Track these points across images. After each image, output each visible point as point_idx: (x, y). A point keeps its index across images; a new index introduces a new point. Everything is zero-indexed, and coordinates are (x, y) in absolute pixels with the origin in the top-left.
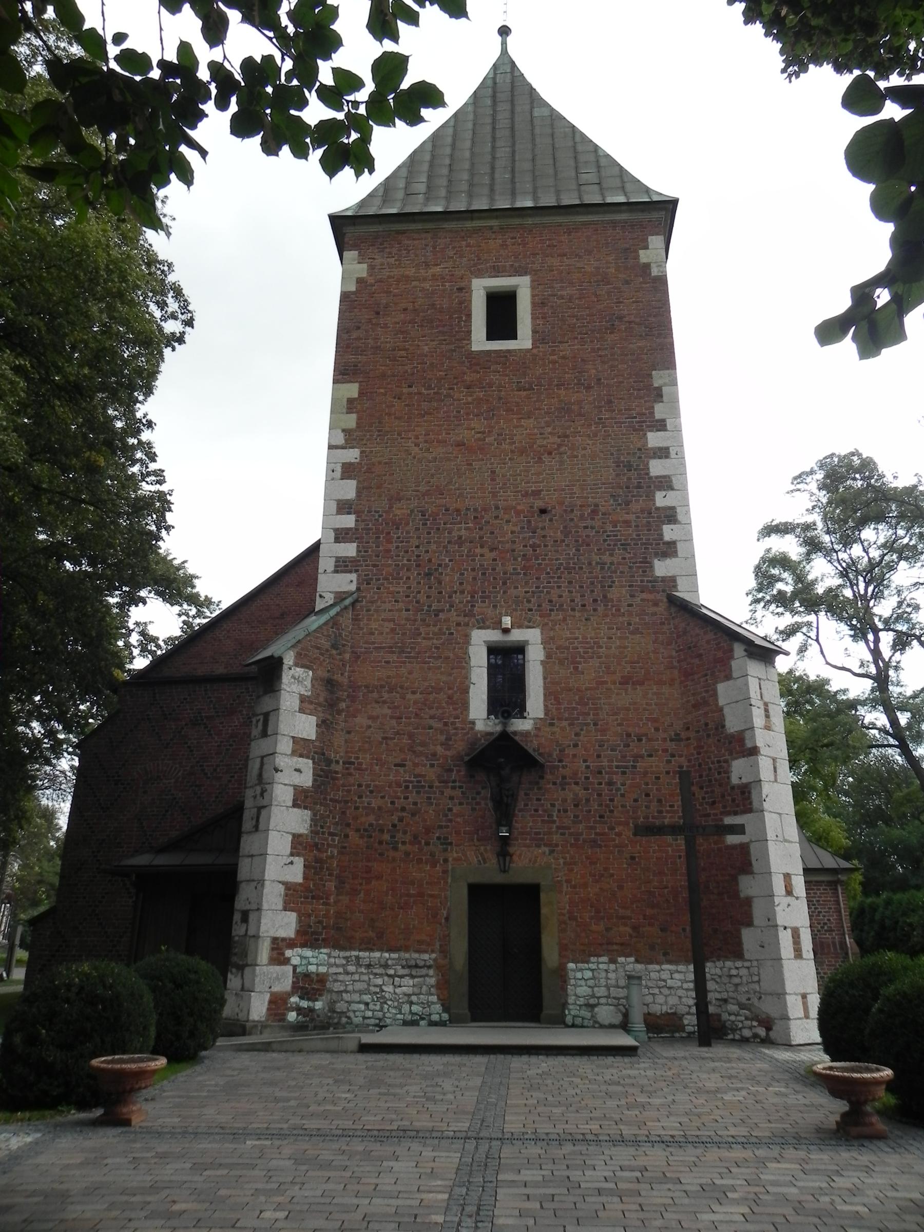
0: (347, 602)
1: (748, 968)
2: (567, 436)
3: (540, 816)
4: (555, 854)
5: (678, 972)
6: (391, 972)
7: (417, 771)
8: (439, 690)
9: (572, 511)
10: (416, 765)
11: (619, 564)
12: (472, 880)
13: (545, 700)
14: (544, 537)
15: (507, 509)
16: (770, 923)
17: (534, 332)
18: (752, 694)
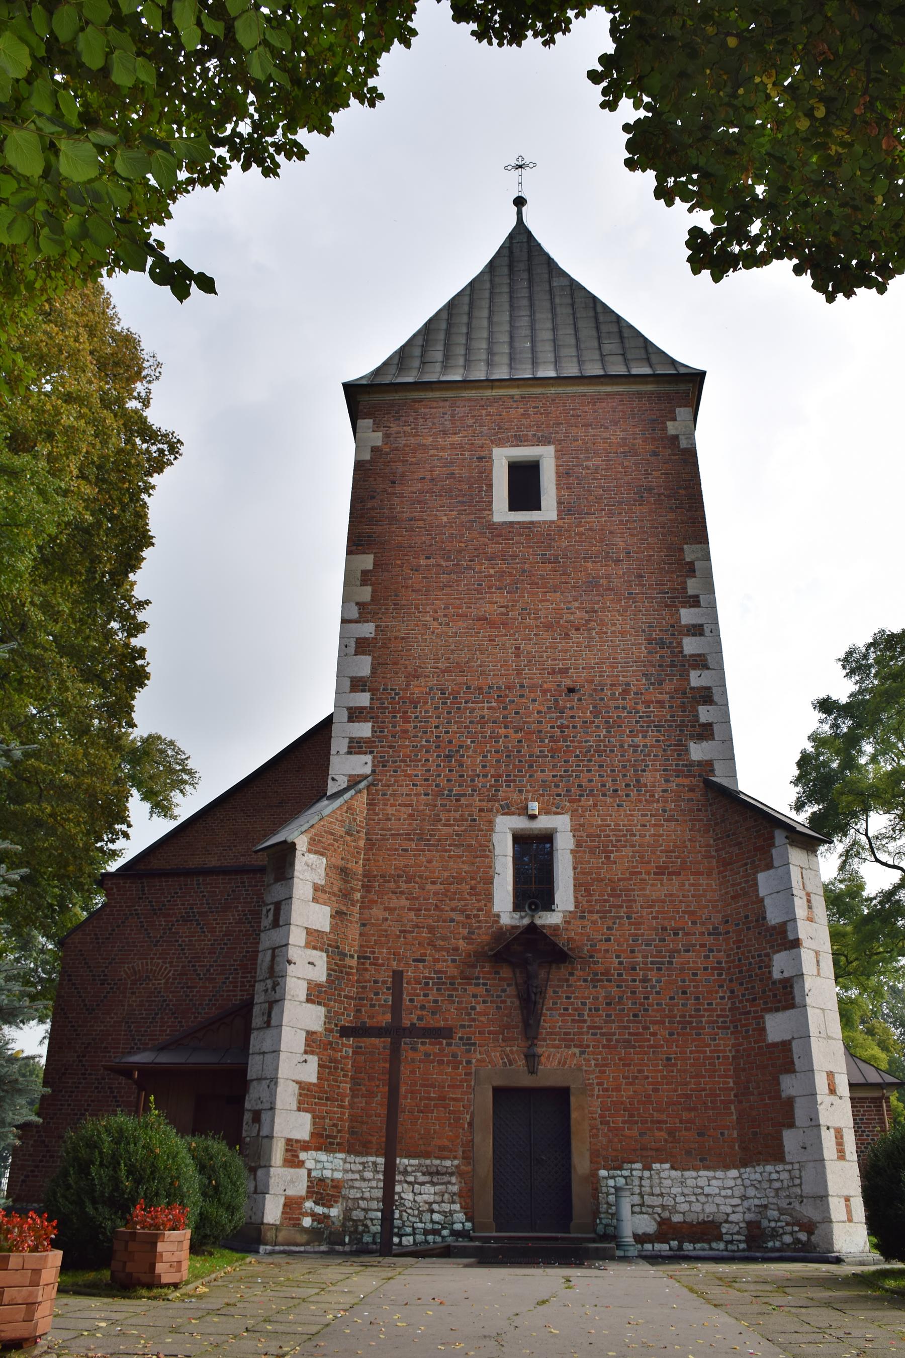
0: (362, 785)
1: (789, 1171)
2: (596, 612)
3: (569, 1015)
4: (586, 1056)
5: (715, 1178)
6: (411, 1179)
7: (438, 966)
8: (460, 880)
9: (602, 690)
10: (436, 960)
11: (652, 746)
12: (499, 1082)
13: (575, 891)
14: (572, 717)
15: (533, 688)
16: (813, 1123)
17: (559, 503)
18: (794, 884)
